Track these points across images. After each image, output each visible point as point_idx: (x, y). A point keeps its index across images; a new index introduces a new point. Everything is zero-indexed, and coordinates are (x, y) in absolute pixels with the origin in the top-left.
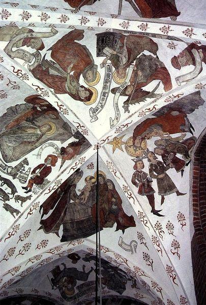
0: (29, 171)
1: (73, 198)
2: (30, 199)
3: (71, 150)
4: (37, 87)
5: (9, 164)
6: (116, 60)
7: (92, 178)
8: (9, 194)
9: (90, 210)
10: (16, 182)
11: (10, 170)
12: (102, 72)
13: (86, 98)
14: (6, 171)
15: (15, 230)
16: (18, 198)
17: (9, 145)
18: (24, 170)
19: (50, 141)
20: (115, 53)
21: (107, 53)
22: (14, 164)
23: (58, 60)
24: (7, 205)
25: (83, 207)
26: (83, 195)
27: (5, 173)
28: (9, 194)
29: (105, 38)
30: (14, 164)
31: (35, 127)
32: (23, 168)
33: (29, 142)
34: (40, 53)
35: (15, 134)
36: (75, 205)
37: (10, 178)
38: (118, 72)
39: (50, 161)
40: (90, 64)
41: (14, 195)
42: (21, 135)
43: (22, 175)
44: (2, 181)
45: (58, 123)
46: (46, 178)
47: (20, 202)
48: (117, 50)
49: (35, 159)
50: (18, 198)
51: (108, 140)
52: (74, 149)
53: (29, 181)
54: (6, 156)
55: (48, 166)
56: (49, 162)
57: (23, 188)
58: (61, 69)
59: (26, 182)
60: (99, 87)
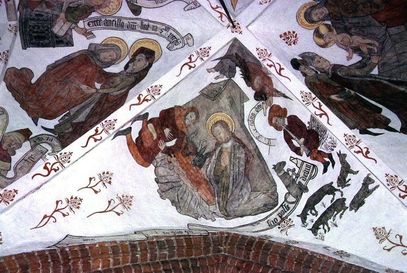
0: (295, 161)
1: (366, 69)
2: (345, 155)
3: (257, 81)
4: (92, 140)
5: (281, 200)
6: (77, 13)
7: (317, 33)
8: (333, 199)
9: (393, 30)
10: (314, 187)
11: (291, 199)
12: (101, 35)
13: (147, 59)
14: (291, 206)
15: (397, 185)
16: (343, 181)
17: (246, 198)
18: (294, 170)
19: (246, 123)
20: (62, 15)
21: (66, 28)
22: (282, 190)
23: (64, 109)
24: (353, 203)
25: (387, 48)
26: (359, 50)
27: (295, 208)
28: (333, 199)
29: (35, 34)
30: (282, 190)
31: (217, 152)
32: (290, 173)
33: (247, 162)
34: (36, 136)
35: (228, 188)
36: (384, 64)
37: (305, 197)
38: (100, 7)
39: (279, 119)
40: (88, 58)
41: (336, 190)
42: (231, 178)
43: (302, 174)
44: (309, 213)
45: (208, 109)
46: (307, 125)
47: (350, 176)
48: (56, 13)
49: (276, 150)
50: (343, 181)
51: (217, 7)
52: (255, 75)
53: (314, 159)
54: (265, 205)
55: (286, 123)
56: (280, 121)
57: (325, 170)
58: (83, 104)
59: (314, 166)
60: (131, 38)
